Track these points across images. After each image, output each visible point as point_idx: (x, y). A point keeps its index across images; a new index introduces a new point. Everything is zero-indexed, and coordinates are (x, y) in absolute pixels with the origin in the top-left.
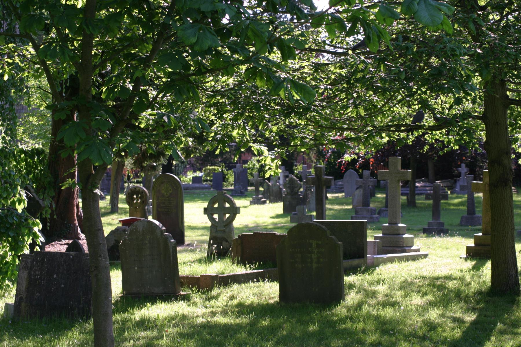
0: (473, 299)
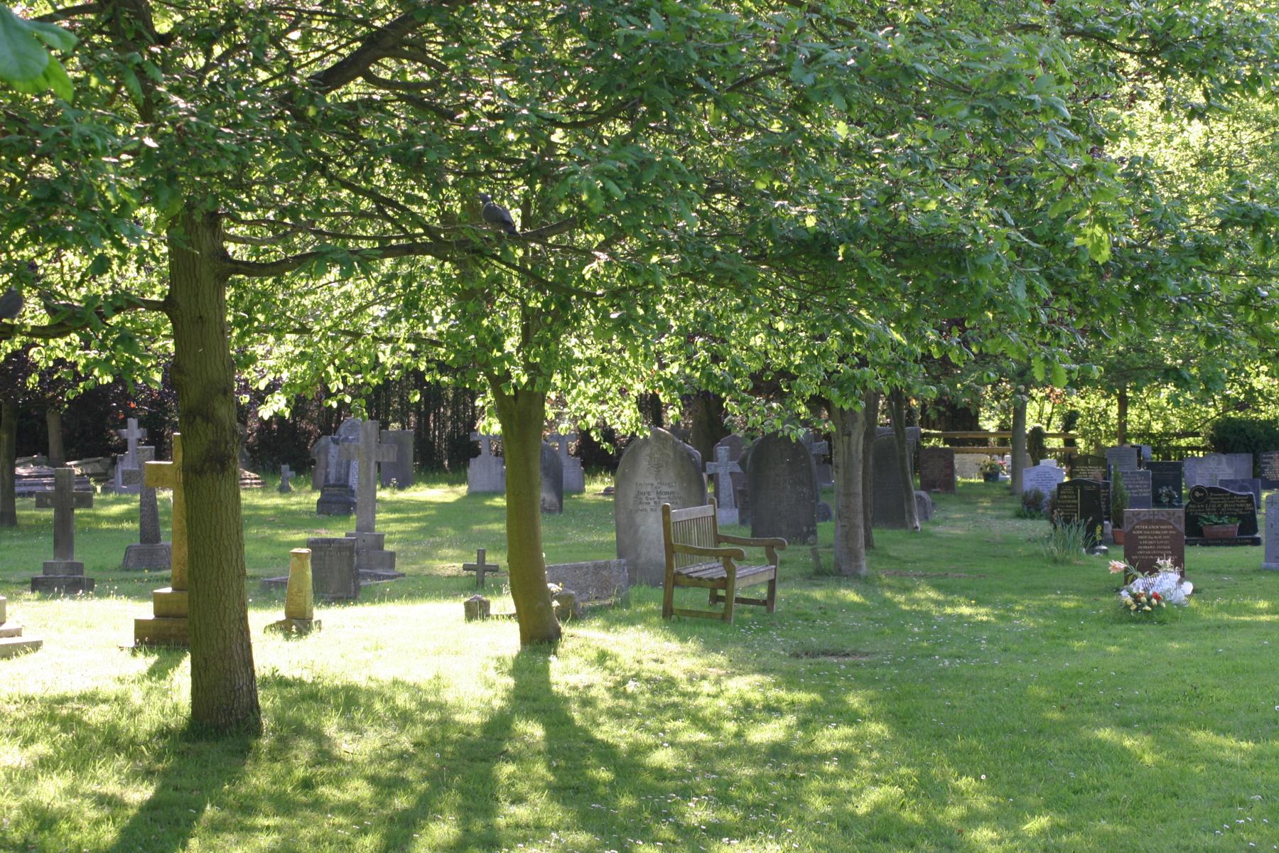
0: (148, 748)
